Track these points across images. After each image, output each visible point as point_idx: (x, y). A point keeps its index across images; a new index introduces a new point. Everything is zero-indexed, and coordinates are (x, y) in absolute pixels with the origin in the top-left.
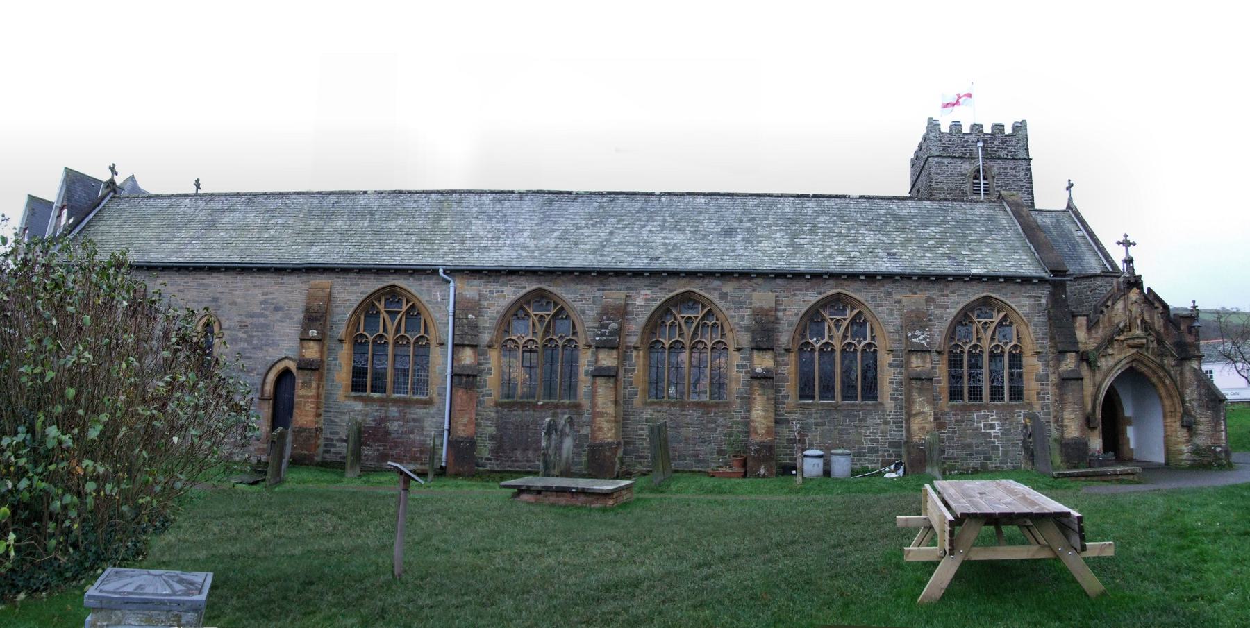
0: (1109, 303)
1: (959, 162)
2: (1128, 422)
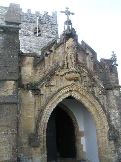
0: (53, 49)
1: (29, 24)
2: (82, 134)
